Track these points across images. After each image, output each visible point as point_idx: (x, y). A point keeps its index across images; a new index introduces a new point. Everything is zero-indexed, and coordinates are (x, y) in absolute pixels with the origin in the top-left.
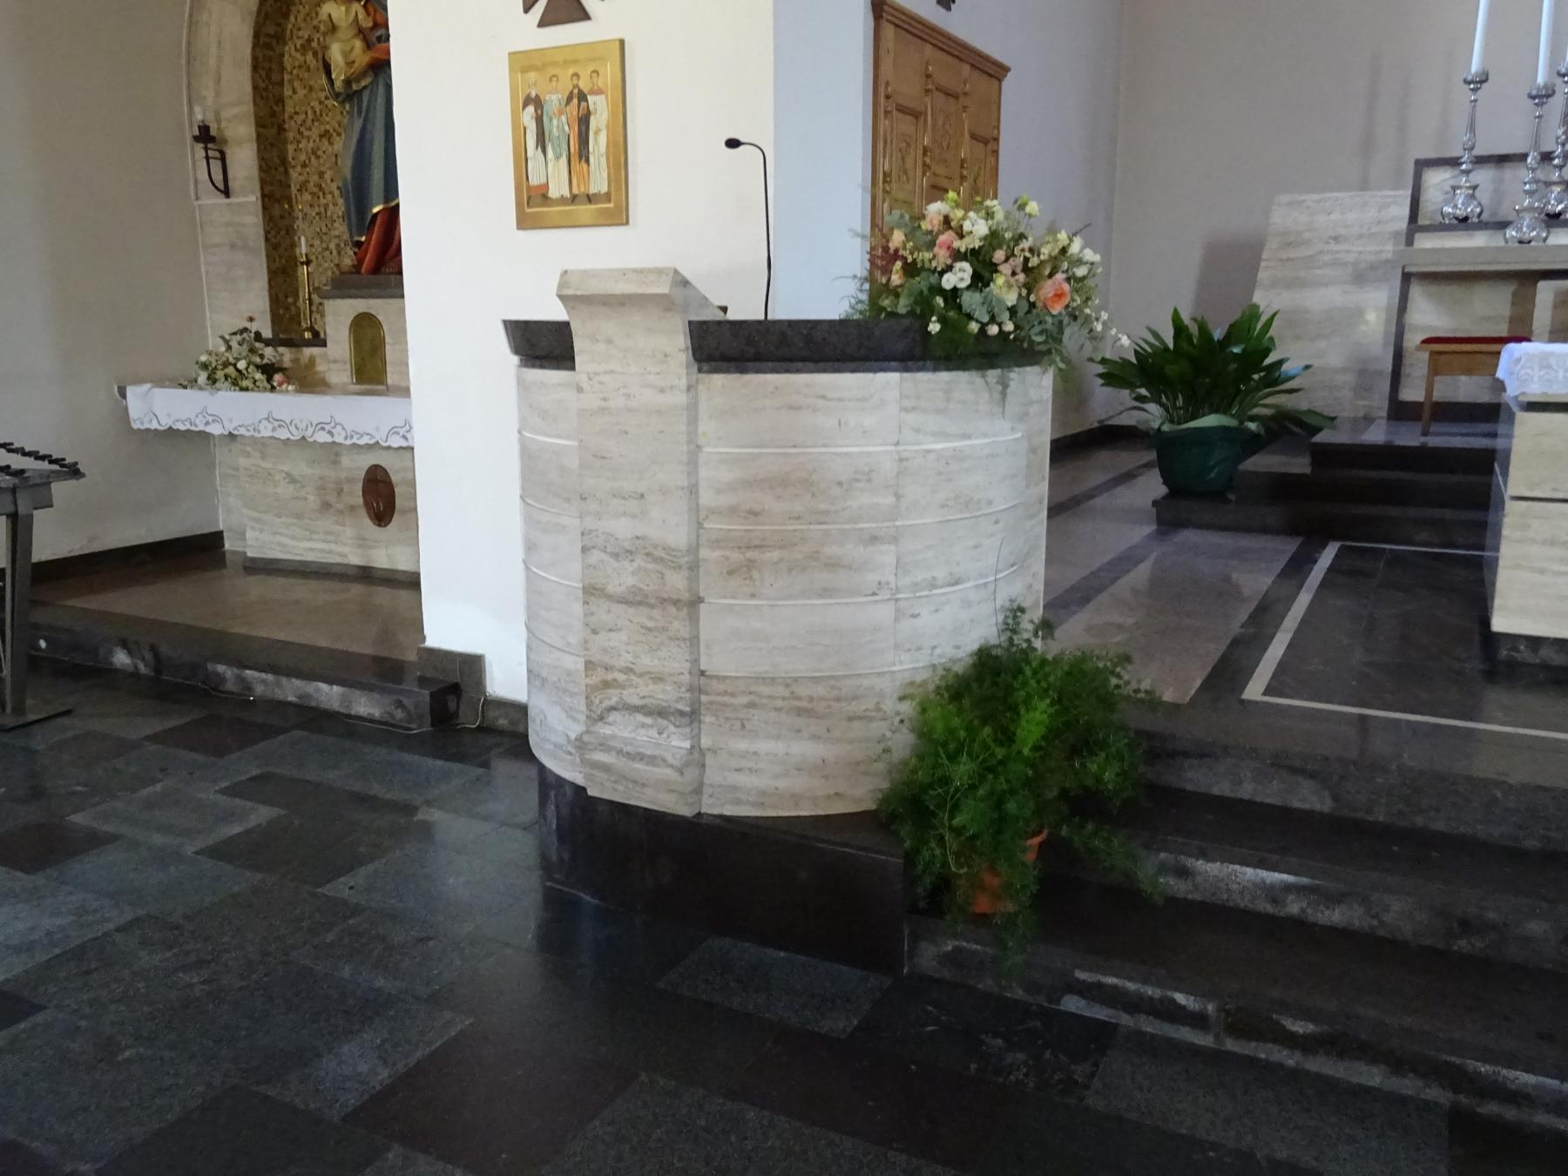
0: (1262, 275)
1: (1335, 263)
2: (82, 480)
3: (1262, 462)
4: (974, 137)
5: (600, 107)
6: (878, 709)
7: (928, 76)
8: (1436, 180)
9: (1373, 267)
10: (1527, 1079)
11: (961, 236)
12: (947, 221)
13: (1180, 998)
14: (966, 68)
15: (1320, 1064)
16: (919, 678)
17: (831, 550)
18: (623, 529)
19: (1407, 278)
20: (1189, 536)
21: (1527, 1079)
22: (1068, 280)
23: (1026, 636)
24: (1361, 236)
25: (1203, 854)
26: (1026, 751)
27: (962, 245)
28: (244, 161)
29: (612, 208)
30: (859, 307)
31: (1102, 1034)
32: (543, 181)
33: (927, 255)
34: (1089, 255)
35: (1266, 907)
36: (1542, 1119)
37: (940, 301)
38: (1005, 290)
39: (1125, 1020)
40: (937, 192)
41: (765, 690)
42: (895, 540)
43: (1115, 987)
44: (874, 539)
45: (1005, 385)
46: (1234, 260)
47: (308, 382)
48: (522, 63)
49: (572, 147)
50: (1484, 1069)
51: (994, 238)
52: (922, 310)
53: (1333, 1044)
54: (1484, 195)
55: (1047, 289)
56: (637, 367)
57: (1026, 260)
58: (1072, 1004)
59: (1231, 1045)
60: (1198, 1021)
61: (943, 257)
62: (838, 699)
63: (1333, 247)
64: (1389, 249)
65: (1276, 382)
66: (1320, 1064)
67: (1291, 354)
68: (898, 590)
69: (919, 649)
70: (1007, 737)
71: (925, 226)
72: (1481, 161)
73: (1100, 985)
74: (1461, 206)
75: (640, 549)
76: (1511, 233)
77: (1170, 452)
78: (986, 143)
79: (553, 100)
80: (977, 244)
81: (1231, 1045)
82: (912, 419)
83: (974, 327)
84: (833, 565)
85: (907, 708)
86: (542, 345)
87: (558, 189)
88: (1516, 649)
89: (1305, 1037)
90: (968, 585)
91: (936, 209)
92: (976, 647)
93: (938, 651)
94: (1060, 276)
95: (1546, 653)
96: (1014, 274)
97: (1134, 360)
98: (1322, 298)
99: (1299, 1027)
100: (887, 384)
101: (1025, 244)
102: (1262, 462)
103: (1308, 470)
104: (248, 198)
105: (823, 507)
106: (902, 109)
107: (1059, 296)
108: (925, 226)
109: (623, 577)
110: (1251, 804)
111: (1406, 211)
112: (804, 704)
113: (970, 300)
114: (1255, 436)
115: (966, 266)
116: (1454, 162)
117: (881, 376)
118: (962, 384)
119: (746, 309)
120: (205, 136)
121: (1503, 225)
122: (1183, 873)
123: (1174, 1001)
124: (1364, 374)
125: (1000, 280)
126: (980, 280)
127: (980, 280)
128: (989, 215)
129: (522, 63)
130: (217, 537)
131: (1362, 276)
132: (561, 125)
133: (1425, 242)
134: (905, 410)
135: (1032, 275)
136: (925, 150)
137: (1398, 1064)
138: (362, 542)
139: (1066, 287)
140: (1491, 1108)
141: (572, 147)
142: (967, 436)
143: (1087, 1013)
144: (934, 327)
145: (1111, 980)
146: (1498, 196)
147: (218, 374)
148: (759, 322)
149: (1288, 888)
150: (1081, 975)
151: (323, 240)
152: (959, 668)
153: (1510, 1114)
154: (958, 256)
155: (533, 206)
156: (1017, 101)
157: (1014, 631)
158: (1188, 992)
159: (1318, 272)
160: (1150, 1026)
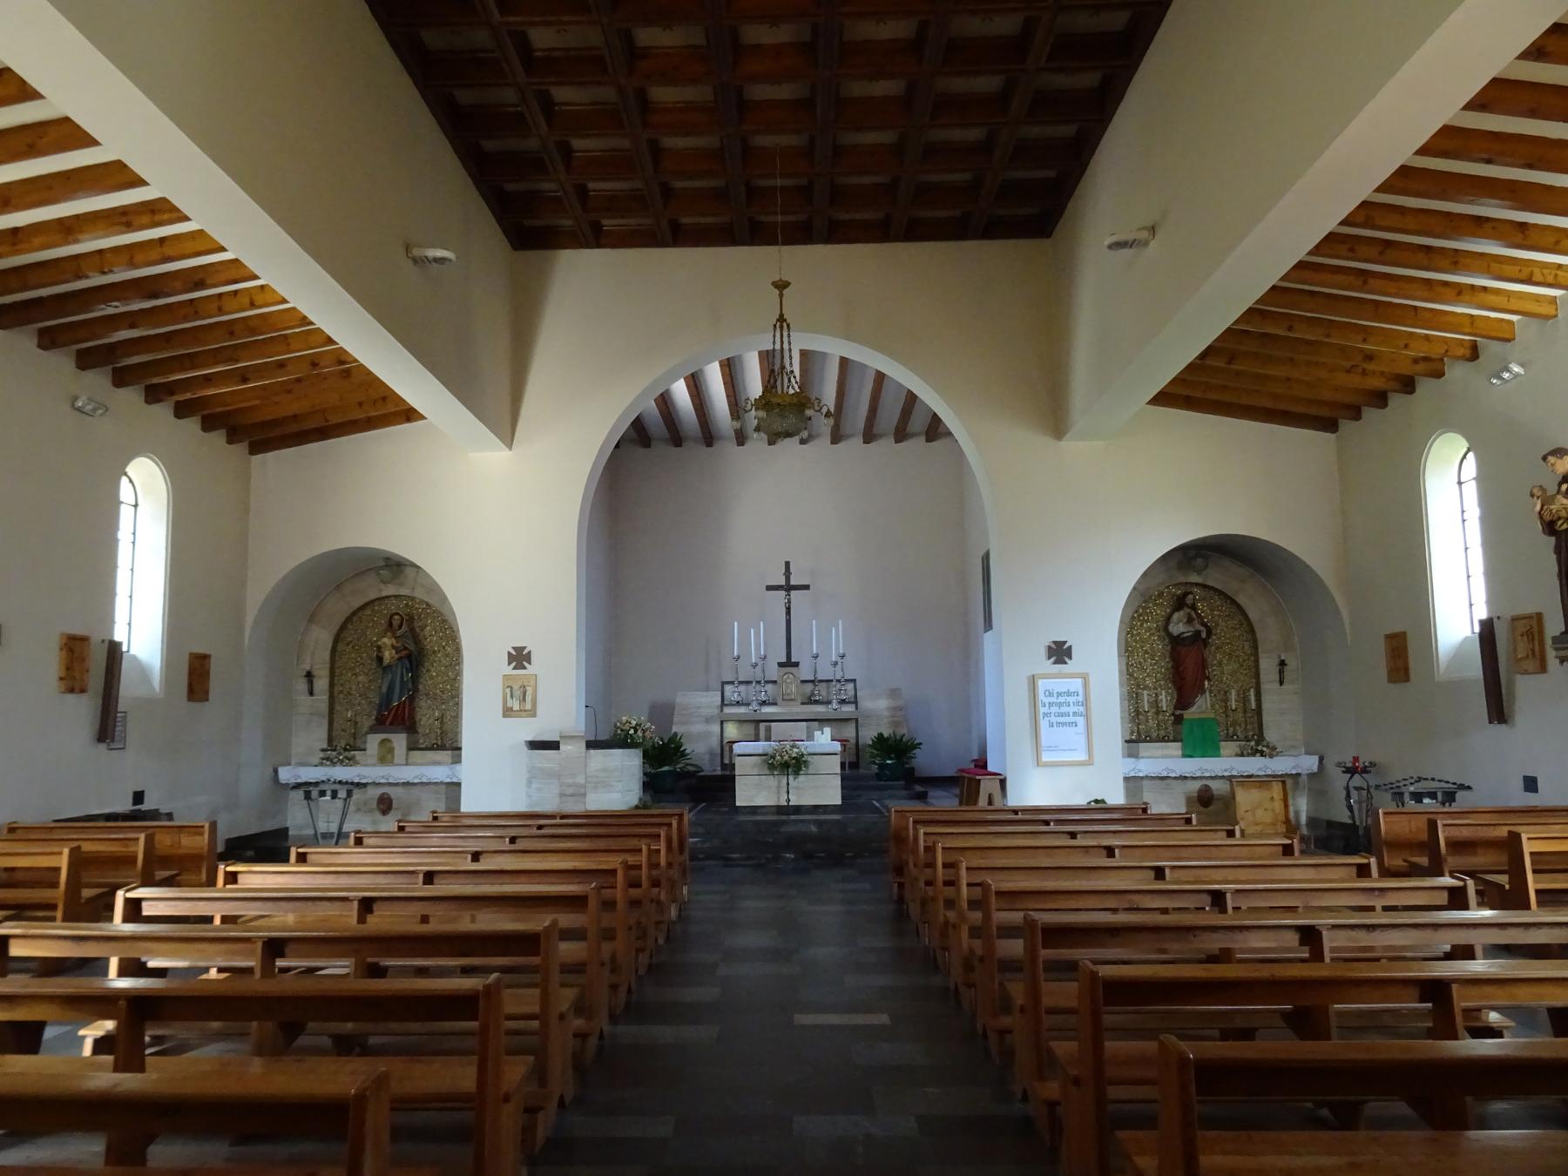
5: (529, 691)
8: (728, 688)
18: (570, 781)
28: (322, 684)
29: (533, 713)
32: (1445, 894)
38: (640, 733)
64: (716, 711)
67: (688, 747)
74: (736, 697)
75: (574, 785)
79: (516, 687)
87: (516, 707)
98: (698, 728)
109: (570, 791)
120: (309, 675)
124: (712, 754)
130: (286, 830)
131: (708, 720)
132: (517, 693)
133: (727, 710)
135: (644, 731)
138: (374, 823)
141: (518, 702)
155: (508, 712)
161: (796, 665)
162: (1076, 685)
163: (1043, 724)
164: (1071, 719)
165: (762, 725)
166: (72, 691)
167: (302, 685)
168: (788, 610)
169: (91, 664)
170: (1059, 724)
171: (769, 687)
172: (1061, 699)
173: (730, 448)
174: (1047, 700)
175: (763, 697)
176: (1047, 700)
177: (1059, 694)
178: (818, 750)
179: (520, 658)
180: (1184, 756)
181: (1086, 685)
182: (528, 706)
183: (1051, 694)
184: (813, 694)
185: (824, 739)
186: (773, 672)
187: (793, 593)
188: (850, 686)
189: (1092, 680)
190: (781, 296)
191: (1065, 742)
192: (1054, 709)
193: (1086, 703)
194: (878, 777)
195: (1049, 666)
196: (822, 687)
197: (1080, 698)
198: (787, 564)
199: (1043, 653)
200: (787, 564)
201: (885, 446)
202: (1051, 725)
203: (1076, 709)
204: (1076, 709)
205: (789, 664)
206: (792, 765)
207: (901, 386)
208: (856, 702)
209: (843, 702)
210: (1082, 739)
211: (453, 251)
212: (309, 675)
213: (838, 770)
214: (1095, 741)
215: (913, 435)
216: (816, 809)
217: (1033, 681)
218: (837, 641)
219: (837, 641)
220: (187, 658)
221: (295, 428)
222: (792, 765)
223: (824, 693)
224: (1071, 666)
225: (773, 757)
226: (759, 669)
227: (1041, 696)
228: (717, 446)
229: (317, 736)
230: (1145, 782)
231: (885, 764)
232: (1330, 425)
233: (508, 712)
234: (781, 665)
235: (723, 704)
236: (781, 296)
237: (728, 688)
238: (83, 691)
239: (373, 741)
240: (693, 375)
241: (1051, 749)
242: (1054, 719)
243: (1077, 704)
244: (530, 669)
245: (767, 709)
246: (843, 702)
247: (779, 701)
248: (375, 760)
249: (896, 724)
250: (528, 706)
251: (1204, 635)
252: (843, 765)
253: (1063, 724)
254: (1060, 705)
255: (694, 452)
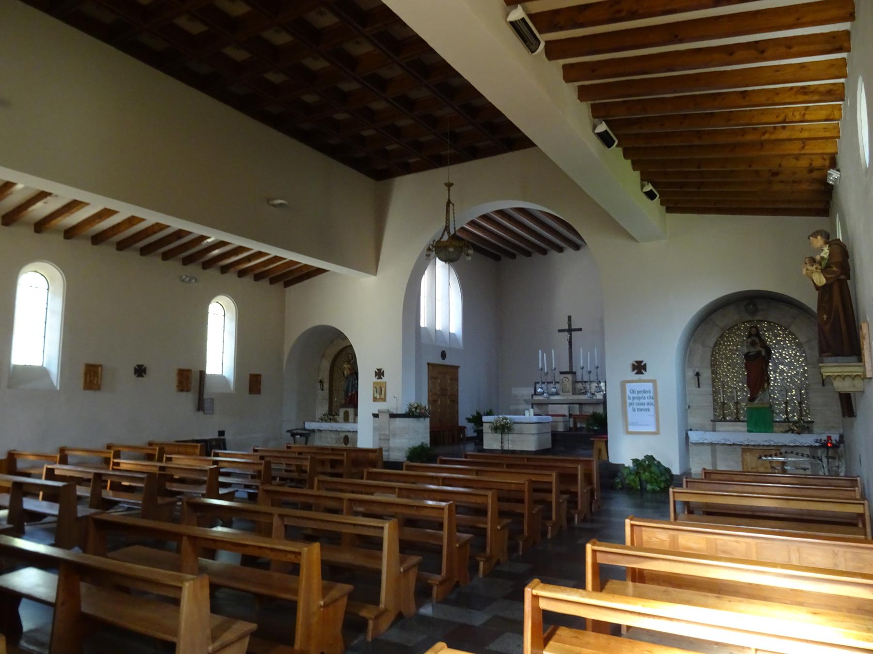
2: (634, 458)
28: (326, 385)
29: (384, 400)
41: (181, 461)
47: (336, 421)
48: (374, 383)
49: (380, 393)
56: (384, 418)
86: (376, 416)
87: (378, 397)
104: (326, 392)
109: (383, 437)
118: (415, 420)
119: (395, 412)
120: (321, 382)
129: (374, 383)
132: (379, 390)
133: (536, 398)
141: (380, 393)
147: (322, 420)
148: (218, 376)
151: (339, 398)
155: (375, 399)
162: (649, 386)
163: (629, 409)
164: (646, 407)
166: (182, 390)
167: (319, 386)
169: (192, 380)
170: (639, 410)
172: (640, 395)
174: (631, 396)
176: (631, 396)
177: (639, 392)
179: (380, 374)
180: (749, 431)
181: (655, 387)
182: (383, 396)
183: (634, 392)
189: (659, 383)
190: (449, 190)
191: (644, 421)
192: (636, 401)
193: (655, 397)
195: (633, 376)
197: (652, 395)
199: (630, 368)
202: (634, 410)
203: (648, 401)
204: (648, 401)
210: (652, 420)
211: (858, 78)
212: (321, 382)
214: (661, 420)
216: (522, 452)
217: (623, 384)
220: (248, 377)
221: (297, 275)
224: (646, 376)
227: (628, 393)
229: (322, 409)
230: (718, 447)
232: (497, 258)
233: (375, 399)
236: (449, 190)
237: (538, 386)
238: (188, 391)
239: (342, 411)
241: (634, 424)
242: (635, 407)
243: (649, 398)
244: (384, 379)
247: (561, 393)
248: (342, 420)
250: (383, 396)
251: (763, 353)
253: (642, 410)
254: (639, 398)
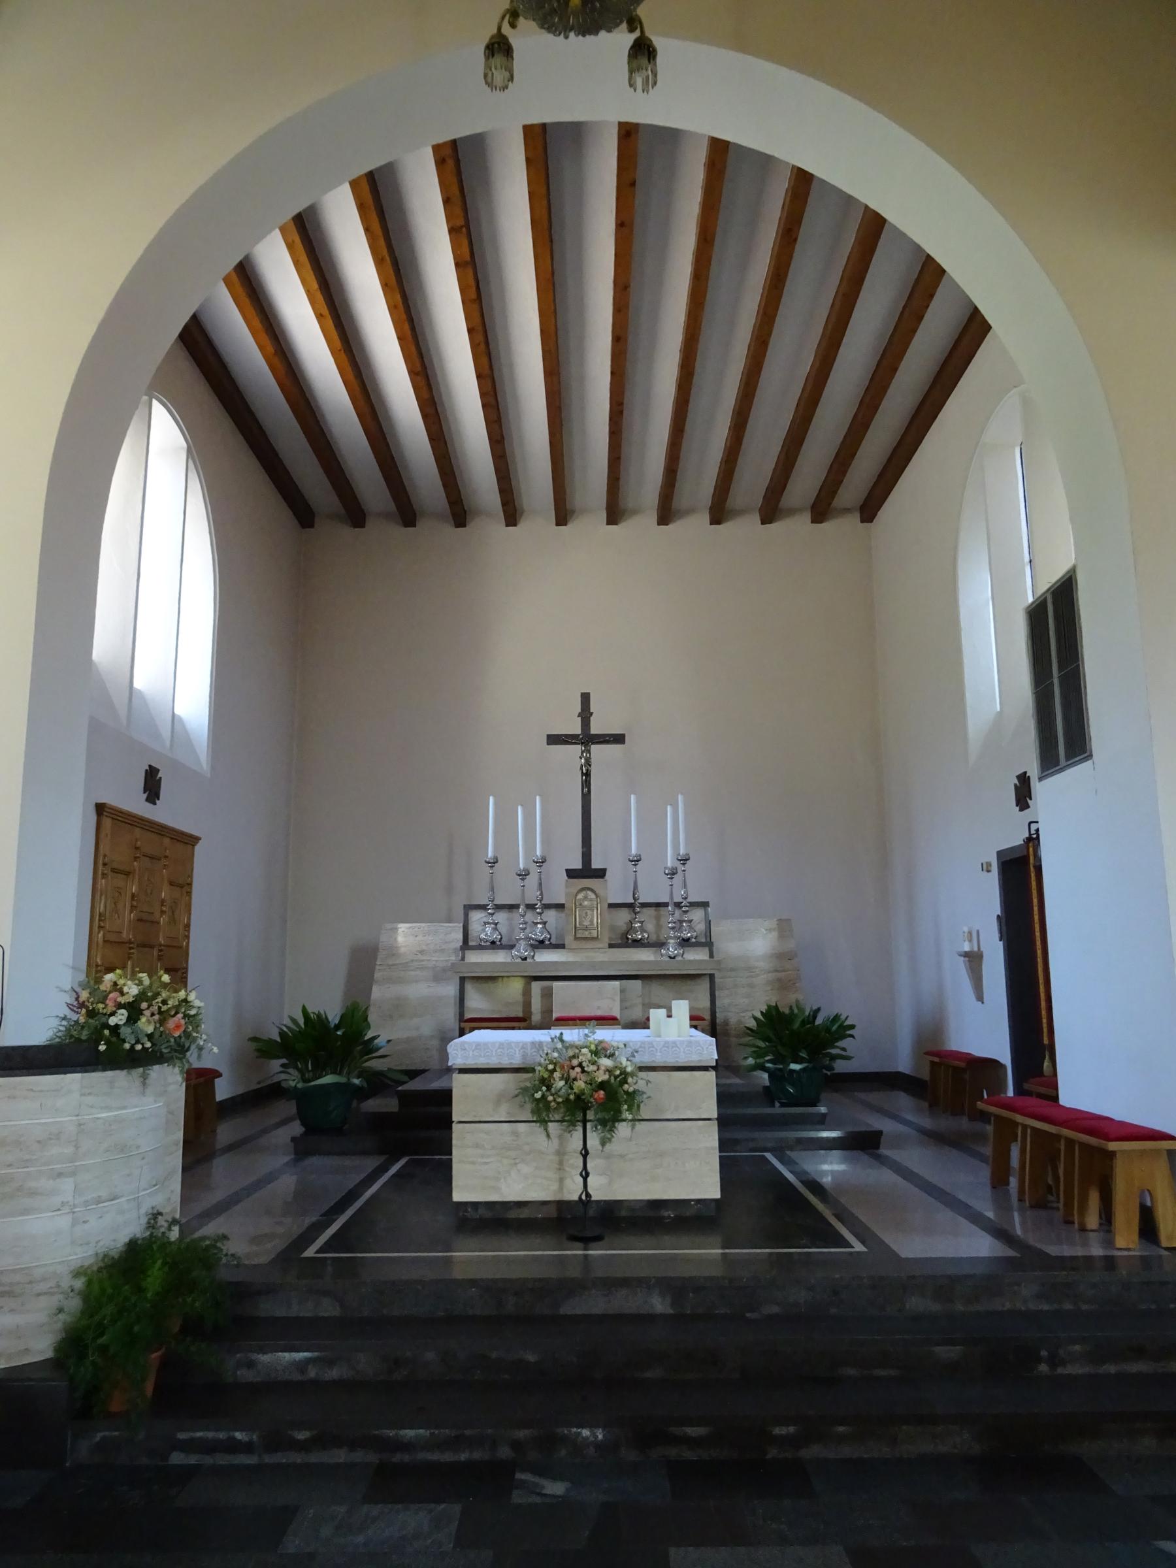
0: (377, 975)
1: (422, 968)
3: (373, 1105)
4: (171, 884)
6: (58, 1286)
7: (137, 848)
8: (477, 917)
9: (444, 970)
10: (409, 1433)
11: (122, 994)
12: (115, 984)
13: (238, 1435)
14: (167, 841)
15: (314, 1458)
16: (87, 1264)
17: (33, 1184)
19: (463, 980)
20: (315, 1161)
21: (409, 1433)
22: (184, 1018)
23: (162, 1230)
24: (435, 951)
25: (263, 1351)
26: (149, 1295)
27: (122, 1000)
30: (60, 1034)
31: (190, 1472)
33: (101, 1006)
34: (197, 1003)
35: (297, 1377)
36: (422, 1456)
37: (107, 1032)
38: (146, 1025)
39: (208, 1460)
40: (110, 970)
42: (73, 1174)
43: (200, 1438)
44: (60, 1175)
45: (144, 1077)
46: (365, 962)
50: (391, 1433)
51: (141, 997)
52: (96, 1037)
53: (322, 1441)
54: (503, 928)
55: (171, 1023)
57: (160, 1008)
58: (177, 1458)
59: (269, 1459)
60: (248, 1448)
61: (111, 1007)
62: (30, 1282)
63: (420, 957)
65: (371, 1051)
66: (314, 1458)
68: (75, 1206)
69: (88, 1244)
70: (140, 1290)
71: (102, 987)
72: (499, 907)
73: (192, 1440)
74: (488, 933)
76: (514, 952)
77: (309, 1105)
78: (181, 886)
80: (131, 1000)
81: (269, 1459)
82: (89, 1100)
83: (127, 1046)
84: (33, 1193)
85: (79, 1284)
88: (466, 1211)
89: (306, 1440)
90: (123, 1199)
91: (109, 977)
92: (127, 1240)
93: (101, 1243)
94: (180, 1016)
95: (482, 1211)
96: (153, 1015)
97: (279, 1040)
99: (302, 1435)
100: (73, 1080)
101: (159, 999)
102: (373, 1105)
103: (396, 1110)
105: (27, 1157)
106: (114, 870)
107: (178, 1027)
108: (102, 987)
110: (297, 1318)
111: (460, 936)
112: (7, 1288)
113: (125, 1032)
114: (358, 1089)
115: (123, 1011)
116: (483, 907)
117: (69, 1076)
118: (120, 1077)
121: (512, 947)
122: (251, 1365)
123: (234, 1438)
125: (143, 1019)
126: (132, 1019)
127: (132, 1019)
128: (140, 983)
133: (473, 957)
134: (83, 1095)
136: (133, 896)
137: (353, 1445)
139: (183, 1022)
140: (398, 1458)
142: (124, 1108)
143: (185, 1462)
144: (102, 1048)
145: (199, 1434)
146: (511, 930)
149: (308, 1361)
150: (181, 1436)
152: (115, 1254)
153: (406, 1458)
154: (120, 1006)
156: (206, 867)
157: (153, 1227)
158: (241, 1430)
159: (413, 973)
160: (223, 1459)
161: (601, 874)
165: (536, 987)
168: (587, 775)
171: (551, 916)
173: (490, 529)
175: (538, 933)
178: (659, 1059)
184: (630, 928)
185: (674, 1032)
186: (559, 889)
187: (594, 748)
188: (697, 915)
194: (769, 1095)
196: (647, 915)
198: (585, 698)
200: (585, 698)
201: (744, 529)
205: (587, 872)
206: (598, 1102)
207: (849, 200)
208: (709, 944)
209: (685, 943)
213: (711, 1109)
215: (792, 512)
218: (675, 832)
219: (675, 832)
222: (598, 1102)
223: (650, 927)
225: (546, 1082)
226: (532, 880)
228: (473, 526)
231: (787, 1064)
234: (571, 874)
235: (466, 945)
236: (587, 856)
240: (370, 176)
245: (546, 957)
246: (685, 943)
247: (569, 940)
249: (783, 985)
252: (724, 1097)
255: (436, 533)
